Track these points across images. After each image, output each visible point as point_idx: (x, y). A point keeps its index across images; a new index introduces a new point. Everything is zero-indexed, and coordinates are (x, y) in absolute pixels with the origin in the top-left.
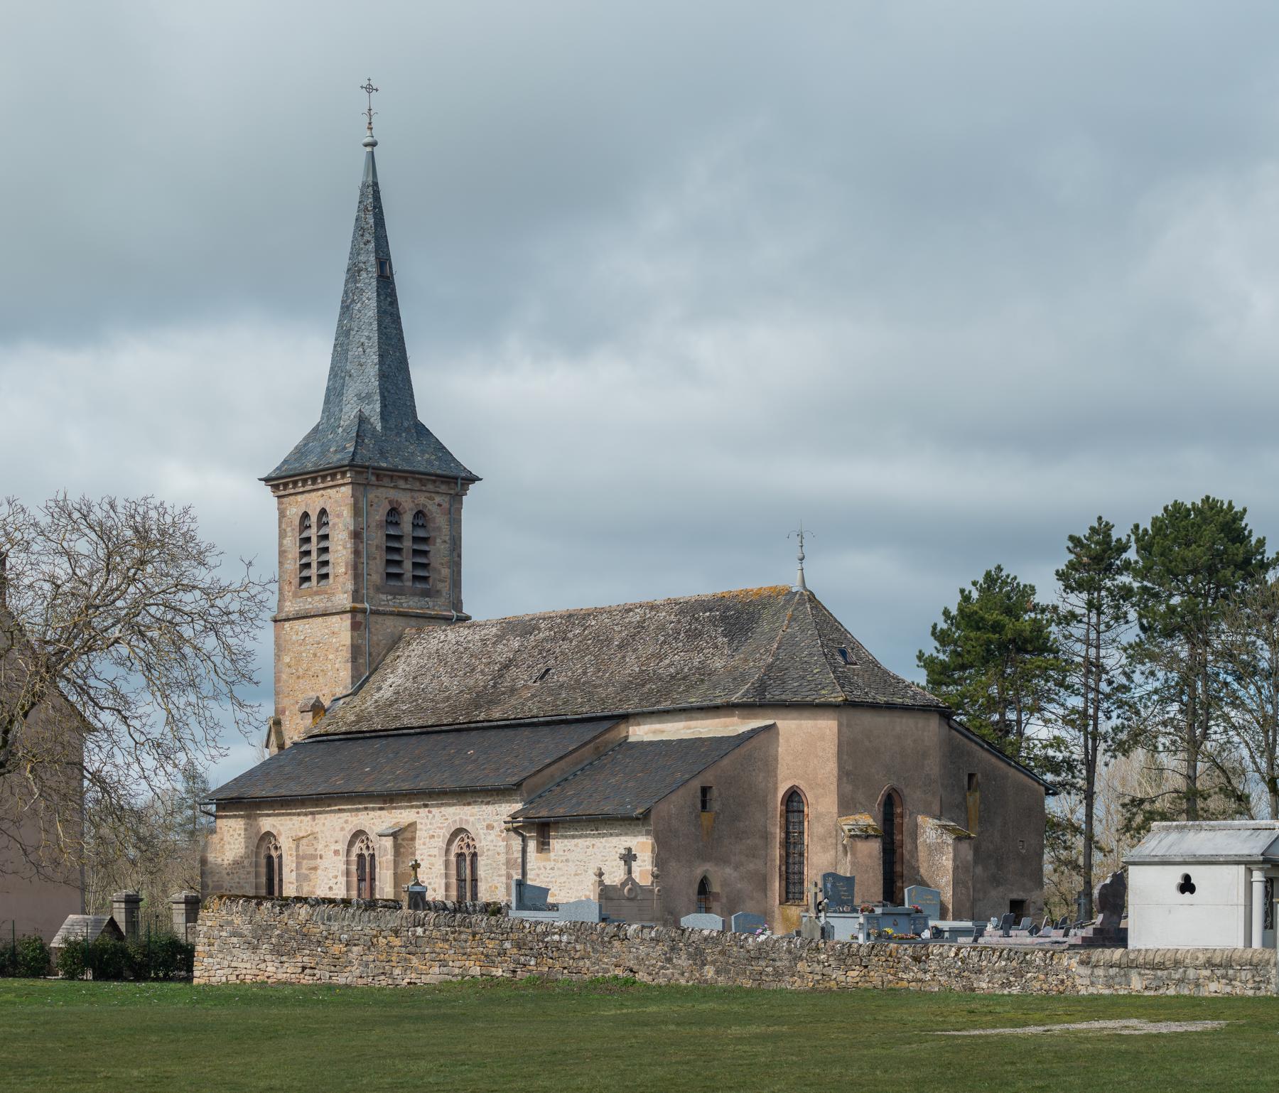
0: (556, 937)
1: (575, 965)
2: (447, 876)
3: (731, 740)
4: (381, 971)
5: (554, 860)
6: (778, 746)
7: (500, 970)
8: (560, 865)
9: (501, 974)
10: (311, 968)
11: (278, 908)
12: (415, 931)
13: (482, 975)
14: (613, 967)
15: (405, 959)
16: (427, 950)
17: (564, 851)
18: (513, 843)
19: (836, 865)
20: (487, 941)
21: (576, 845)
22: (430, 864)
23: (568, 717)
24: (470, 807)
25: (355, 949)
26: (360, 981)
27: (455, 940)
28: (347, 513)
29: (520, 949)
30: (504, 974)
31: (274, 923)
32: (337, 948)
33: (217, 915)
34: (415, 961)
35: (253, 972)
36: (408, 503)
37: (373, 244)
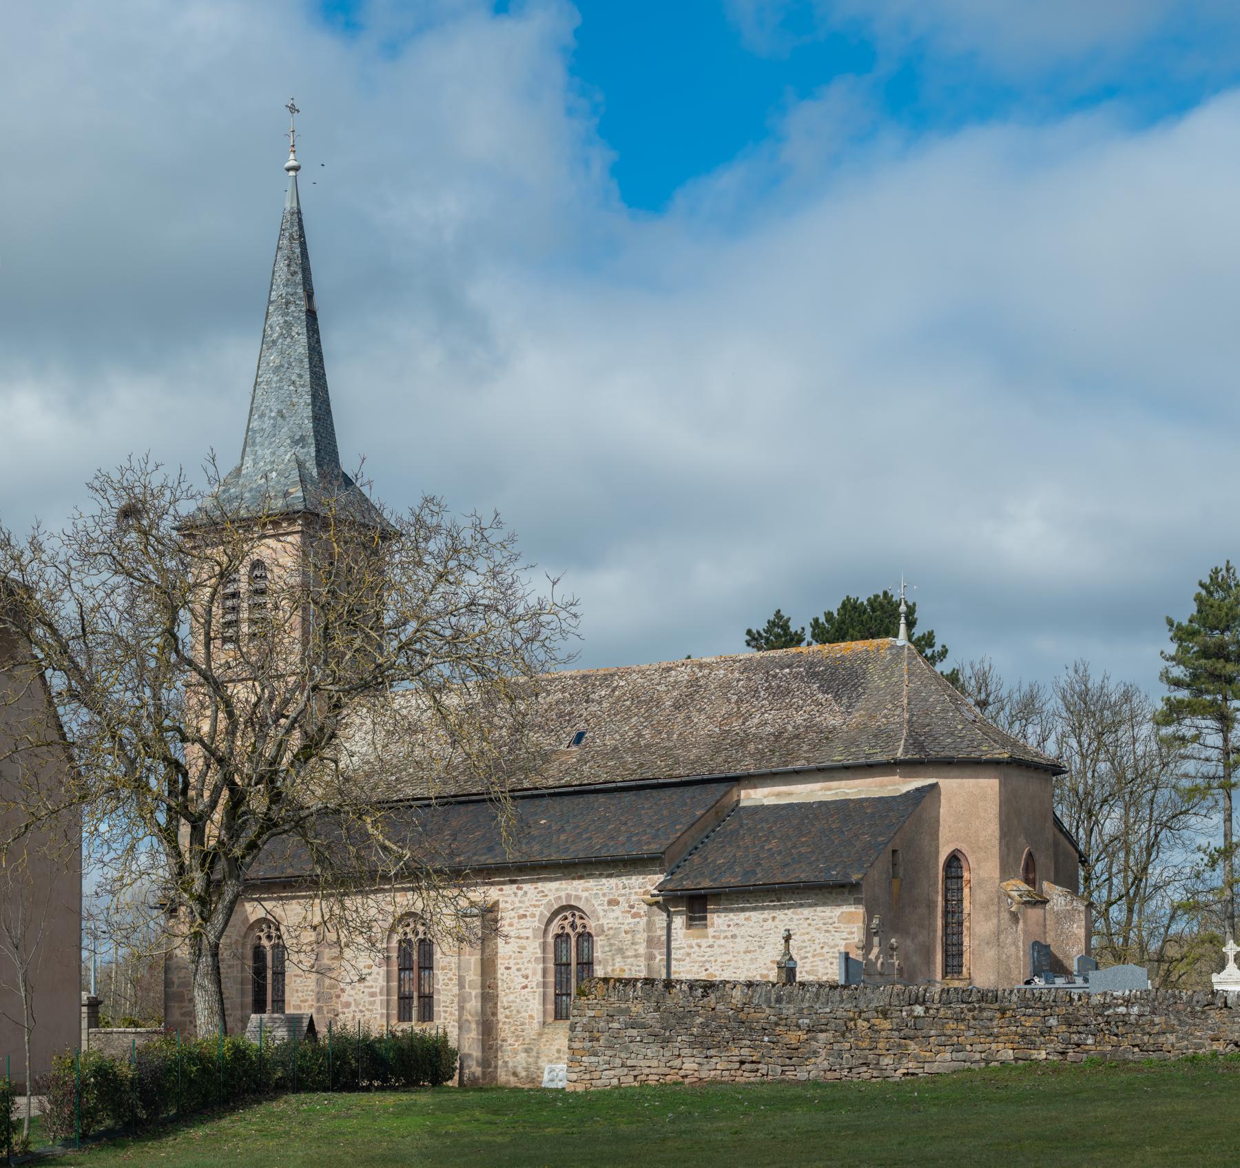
0: (1122, 1010)
1: (1151, 1041)
2: (544, 960)
3: (898, 800)
4: (861, 1061)
5: (714, 937)
6: (940, 807)
7: (1044, 1052)
8: (722, 942)
9: (1044, 1057)
10: (753, 1062)
11: (701, 990)
12: (912, 1011)
13: (1016, 1059)
14: (1209, 1041)
15: (899, 1045)
16: (933, 1032)
17: (729, 926)
18: (656, 918)
19: (999, 934)
20: (1023, 1018)
21: (747, 919)
22: (519, 947)
23: (660, 781)
24: (582, 881)
25: (822, 1036)
26: (830, 1075)
27: (974, 1018)
29: (1070, 1025)
30: (1050, 1057)
31: (695, 1009)
32: (793, 1037)
33: (602, 1002)
34: (913, 1047)
35: (660, 1071)
37: (300, 276)
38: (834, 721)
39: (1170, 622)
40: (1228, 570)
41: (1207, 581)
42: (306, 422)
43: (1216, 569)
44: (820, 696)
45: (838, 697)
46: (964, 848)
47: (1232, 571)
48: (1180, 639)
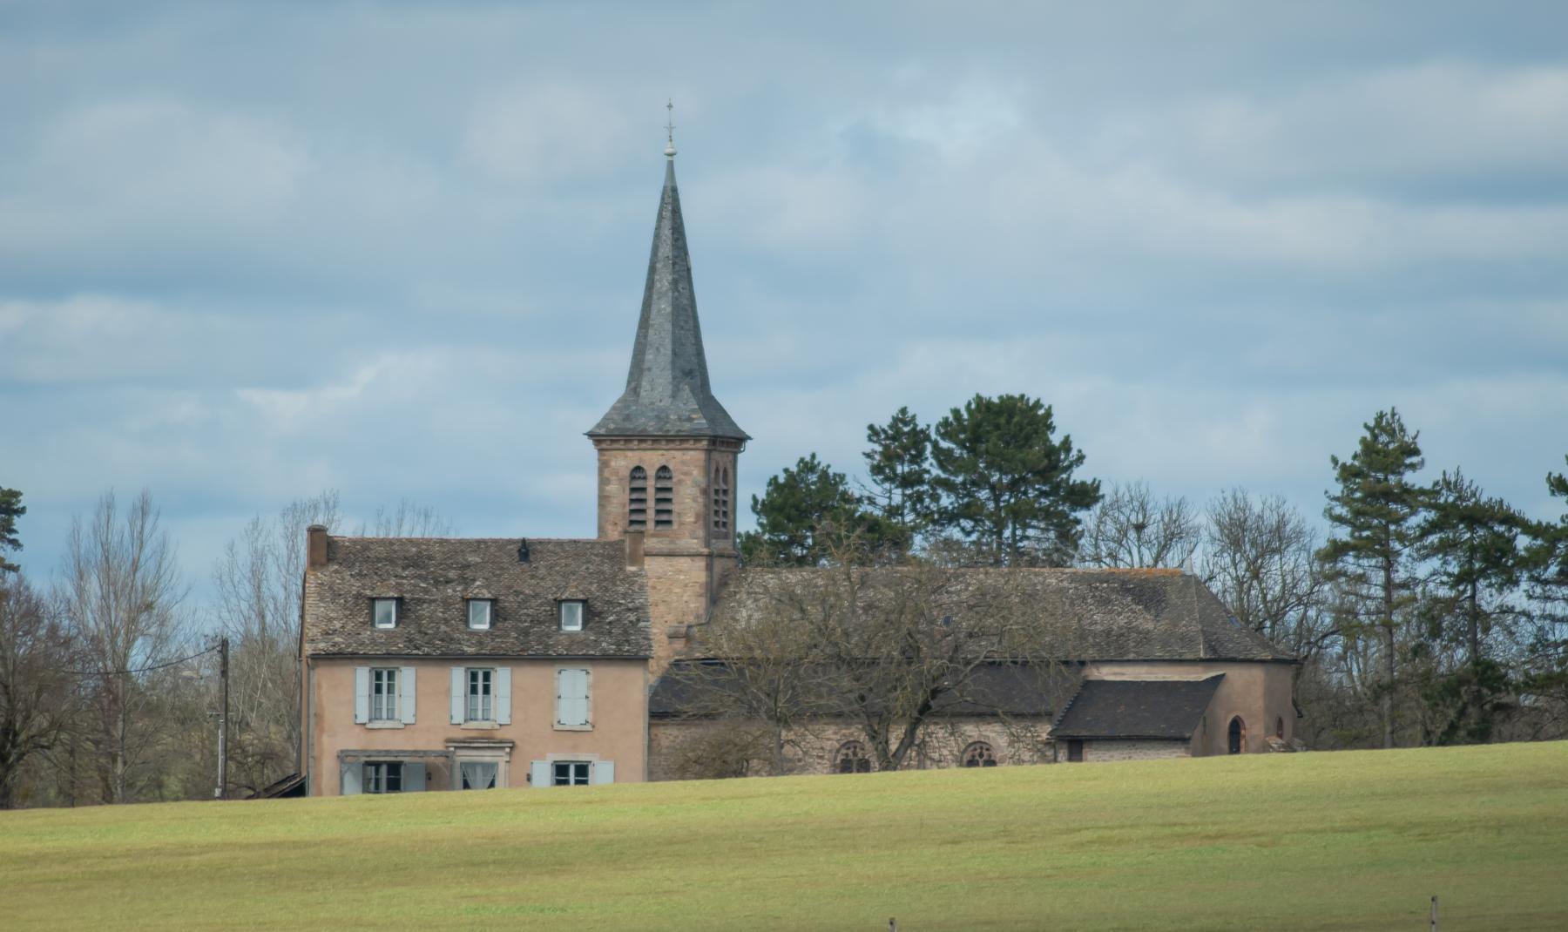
28: (697, 474)
36: (652, 459)
38: (1150, 626)
39: (1335, 461)
40: (1393, 415)
41: (1372, 423)
42: (693, 358)
43: (1381, 413)
44: (1134, 606)
45: (1147, 608)
46: (1241, 714)
47: (1397, 417)
48: (1345, 480)
